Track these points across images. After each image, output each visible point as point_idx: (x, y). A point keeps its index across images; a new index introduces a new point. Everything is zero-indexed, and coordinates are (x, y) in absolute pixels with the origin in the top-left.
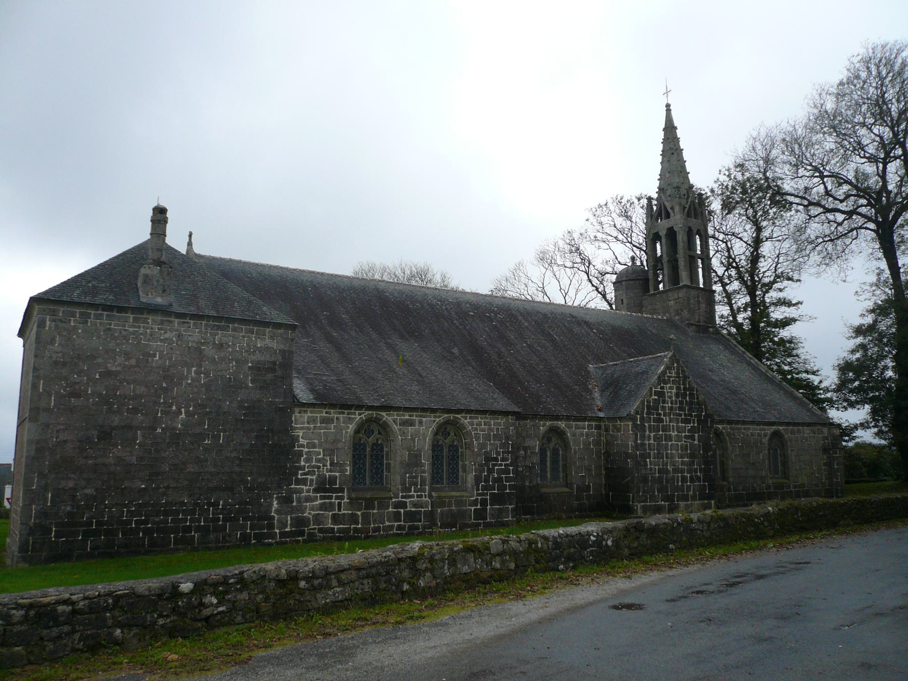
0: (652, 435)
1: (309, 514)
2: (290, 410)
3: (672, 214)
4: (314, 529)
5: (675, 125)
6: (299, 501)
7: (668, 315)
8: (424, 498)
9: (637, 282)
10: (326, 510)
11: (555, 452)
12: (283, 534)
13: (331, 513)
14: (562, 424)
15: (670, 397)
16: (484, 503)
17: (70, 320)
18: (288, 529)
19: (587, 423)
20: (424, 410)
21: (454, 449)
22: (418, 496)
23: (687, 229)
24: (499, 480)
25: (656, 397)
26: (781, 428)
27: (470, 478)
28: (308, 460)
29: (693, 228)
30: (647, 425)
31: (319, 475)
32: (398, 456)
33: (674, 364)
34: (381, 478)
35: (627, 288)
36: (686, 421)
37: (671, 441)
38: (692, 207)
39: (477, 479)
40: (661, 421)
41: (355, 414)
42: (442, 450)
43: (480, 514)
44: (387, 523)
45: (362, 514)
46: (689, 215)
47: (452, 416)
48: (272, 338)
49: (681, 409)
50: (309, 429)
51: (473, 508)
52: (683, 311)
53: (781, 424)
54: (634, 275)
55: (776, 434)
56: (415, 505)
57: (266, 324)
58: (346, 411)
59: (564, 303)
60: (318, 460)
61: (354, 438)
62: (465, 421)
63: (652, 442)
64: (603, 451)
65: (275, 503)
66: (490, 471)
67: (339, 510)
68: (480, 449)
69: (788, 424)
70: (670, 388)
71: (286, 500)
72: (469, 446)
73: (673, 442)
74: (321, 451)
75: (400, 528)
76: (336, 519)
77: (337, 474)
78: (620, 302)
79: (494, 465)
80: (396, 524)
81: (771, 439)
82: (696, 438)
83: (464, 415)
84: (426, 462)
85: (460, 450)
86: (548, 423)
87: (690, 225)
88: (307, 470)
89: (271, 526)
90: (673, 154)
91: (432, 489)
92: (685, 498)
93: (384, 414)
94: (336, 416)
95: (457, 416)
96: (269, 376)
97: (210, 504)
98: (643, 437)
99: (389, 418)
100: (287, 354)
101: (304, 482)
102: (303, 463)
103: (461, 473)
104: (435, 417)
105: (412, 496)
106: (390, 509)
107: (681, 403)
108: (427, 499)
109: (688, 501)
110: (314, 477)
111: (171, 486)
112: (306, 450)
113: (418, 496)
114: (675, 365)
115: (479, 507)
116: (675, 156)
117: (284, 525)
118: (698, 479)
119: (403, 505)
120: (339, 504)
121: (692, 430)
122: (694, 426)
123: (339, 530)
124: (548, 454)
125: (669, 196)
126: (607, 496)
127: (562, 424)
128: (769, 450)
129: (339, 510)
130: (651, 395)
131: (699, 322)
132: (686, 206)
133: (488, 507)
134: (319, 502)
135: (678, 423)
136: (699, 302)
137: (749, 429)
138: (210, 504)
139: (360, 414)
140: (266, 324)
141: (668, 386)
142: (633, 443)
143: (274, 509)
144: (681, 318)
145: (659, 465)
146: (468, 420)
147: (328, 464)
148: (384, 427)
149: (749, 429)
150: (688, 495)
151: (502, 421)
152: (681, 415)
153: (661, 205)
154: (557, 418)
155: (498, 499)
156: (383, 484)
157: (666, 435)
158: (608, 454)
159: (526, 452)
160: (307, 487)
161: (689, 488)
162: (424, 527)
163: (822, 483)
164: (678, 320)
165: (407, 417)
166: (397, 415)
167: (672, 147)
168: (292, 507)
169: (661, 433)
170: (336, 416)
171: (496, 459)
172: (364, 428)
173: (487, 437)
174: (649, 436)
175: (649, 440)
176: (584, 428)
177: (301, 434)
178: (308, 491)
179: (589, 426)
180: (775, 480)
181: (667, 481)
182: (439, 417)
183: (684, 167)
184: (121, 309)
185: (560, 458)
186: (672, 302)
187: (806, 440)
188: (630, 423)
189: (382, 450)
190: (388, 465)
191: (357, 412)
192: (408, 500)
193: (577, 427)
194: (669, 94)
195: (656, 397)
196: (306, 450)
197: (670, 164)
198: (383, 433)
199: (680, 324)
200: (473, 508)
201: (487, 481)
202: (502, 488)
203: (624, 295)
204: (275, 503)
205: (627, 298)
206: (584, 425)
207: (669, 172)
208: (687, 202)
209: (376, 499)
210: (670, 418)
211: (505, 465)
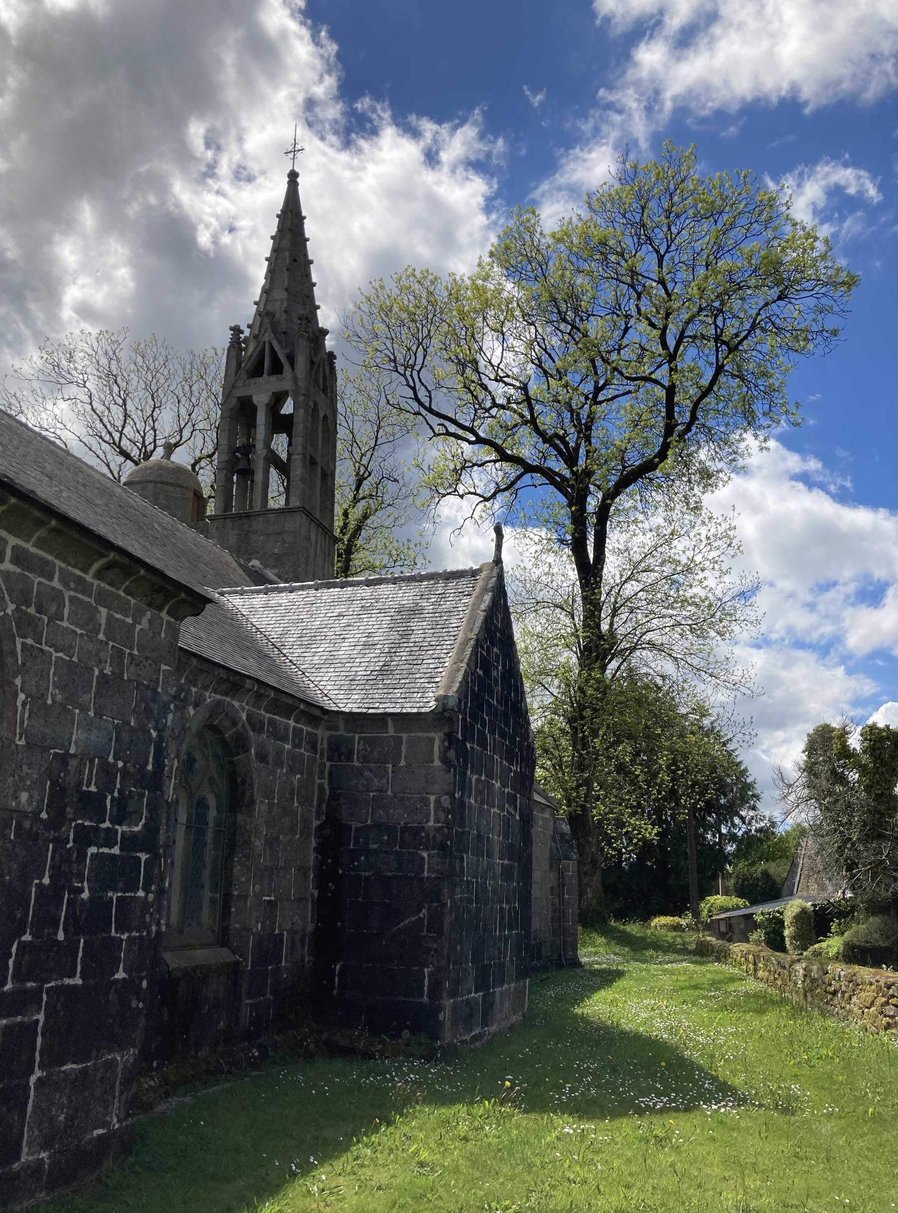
79: (85, 837)
127: (241, 708)
142: (446, 801)
153: (263, 350)
188: (437, 738)
211: (130, 842)
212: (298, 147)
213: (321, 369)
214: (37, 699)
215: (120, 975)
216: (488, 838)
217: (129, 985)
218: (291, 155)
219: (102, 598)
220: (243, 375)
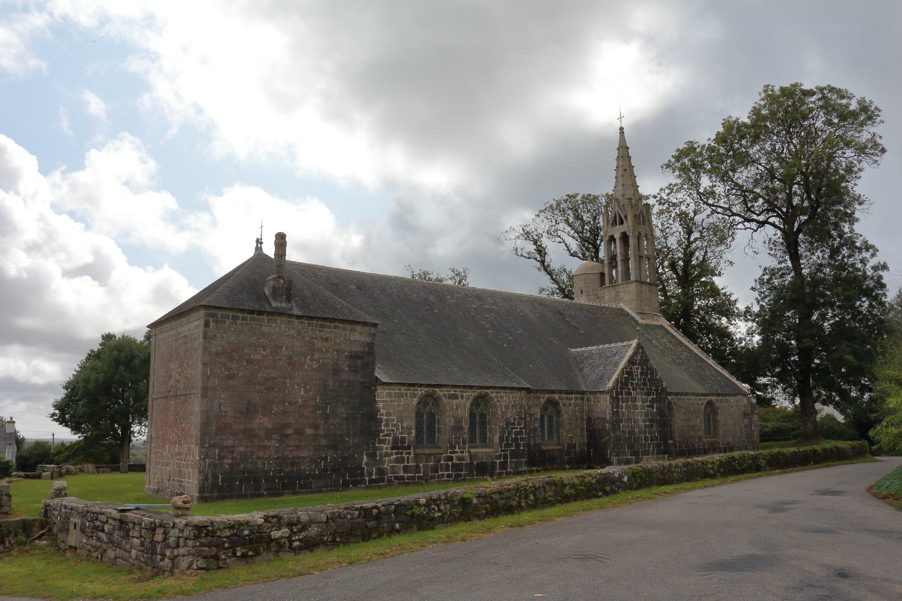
0: (624, 404)
1: (388, 465)
2: (375, 388)
3: (625, 221)
4: (392, 477)
6: (381, 456)
8: (464, 454)
10: (398, 463)
11: (550, 418)
12: (371, 481)
13: (402, 465)
14: (556, 396)
15: (637, 376)
16: (505, 457)
17: (226, 321)
18: (374, 477)
19: (574, 396)
20: (464, 387)
21: (483, 416)
22: (461, 452)
24: (516, 439)
25: (627, 376)
26: (713, 398)
27: (496, 439)
28: (387, 425)
30: (620, 397)
31: (394, 437)
32: (447, 422)
34: (434, 438)
36: (648, 394)
37: (637, 409)
38: (641, 216)
39: (501, 439)
40: (631, 394)
41: (418, 390)
42: (475, 417)
43: (503, 466)
44: (440, 473)
45: (423, 466)
47: (483, 391)
48: (361, 333)
49: (645, 384)
50: (386, 401)
51: (498, 461)
53: (713, 395)
55: (710, 403)
56: (459, 458)
57: (358, 323)
58: (412, 388)
60: (393, 426)
61: (417, 408)
62: (493, 394)
63: (624, 410)
64: (585, 418)
65: (365, 457)
66: (510, 433)
67: (408, 463)
68: (503, 417)
69: (718, 395)
70: (637, 369)
71: (372, 456)
72: (494, 414)
73: (639, 410)
74: (395, 418)
75: (448, 476)
76: (406, 469)
77: (406, 436)
78: (580, 292)
79: (512, 429)
80: (446, 473)
81: (706, 408)
82: (655, 407)
83: (491, 390)
84: (466, 426)
85: (488, 417)
86: (547, 396)
88: (386, 433)
89: (362, 474)
91: (470, 447)
92: (647, 453)
93: (437, 390)
94: (405, 392)
95: (487, 391)
96: (359, 362)
97: (322, 459)
98: (617, 407)
99: (441, 393)
100: (371, 345)
101: (383, 442)
102: (383, 428)
103: (488, 434)
104: (472, 392)
105: (457, 452)
106: (442, 462)
107: (645, 379)
108: (467, 454)
109: (649, 455)
110: (391, 438)
112: (385, 418)
113: (461, 452)
115: (502, 460)
117: (370, 474)
118: (656, 438)
119: (451, 459)
120: (408, 458)
121: (652, 401)
122: (653, 398)
123: (408, 478)
124: (546, 420)
126: (589, 451)
127: (556, 396)
128: (704, 416)
129: (408, 463)
130: (623, 374)
133: (509, 460)
134: (394, 456)
135: (642, 396)
137: (690, 399)
138: (322, 459)
139: (421, 390)
140: (358, 323)
141: (635, 367)
142: (610, 412)
143: (364, 462)
145: (628, 428)
146: (495, 394)
147: (400, 428)
148: (436, 400)
149: (690, 399)
150: (648, 451)
151: (518, 394)
152: (644, 389)
153: (616, 214)
154: (553, 392)
155: (514, 454)
156: (435, 443)
157: (633, 405)
158: (589, 419)
159: (531, 418)
160: (386, 446)
161: (649, 445)
162: (465, 475)
163: (742, 441)
165: (453, 392)
166: (447, 391)
168: (376, 460)
169: (630, 403)
170: (405, 392)
171: (513, 424)
172: (423, 402)
173: (507, 407)
174: (622, 405)
175: (622, 409)
176: (572, 399)
177: (381, 406)
178: (387, 449)
179: (576, 398)
180: (708, 440)
181: (635, 440)
182: (475, 392)
184: (260, 313)
185: (554, 423)
187: (732, 407)
188: (608, 396)
189: (434, 418)
190: (439, 429)
191: (419, 389)
192: (454, 455)
193: (567, 399)
194: (619, 117)
195: (627, 376)
196: (385, 418)
198: (435, 404)
200: (498, 461)
201: (507, 440)
202: (518, 446)
204: (365, 457)
206: (572, 397)
209: (432, 454)
210: (636, 392)
211: (520, 428)
212: (622, 116)
213: (641, 216)
214: (501, 411)
215: (522, 448)
216: (634, 419)
217: (523, 450)
218: (622, 116)
219: (510, 393)
220: (610, 225)
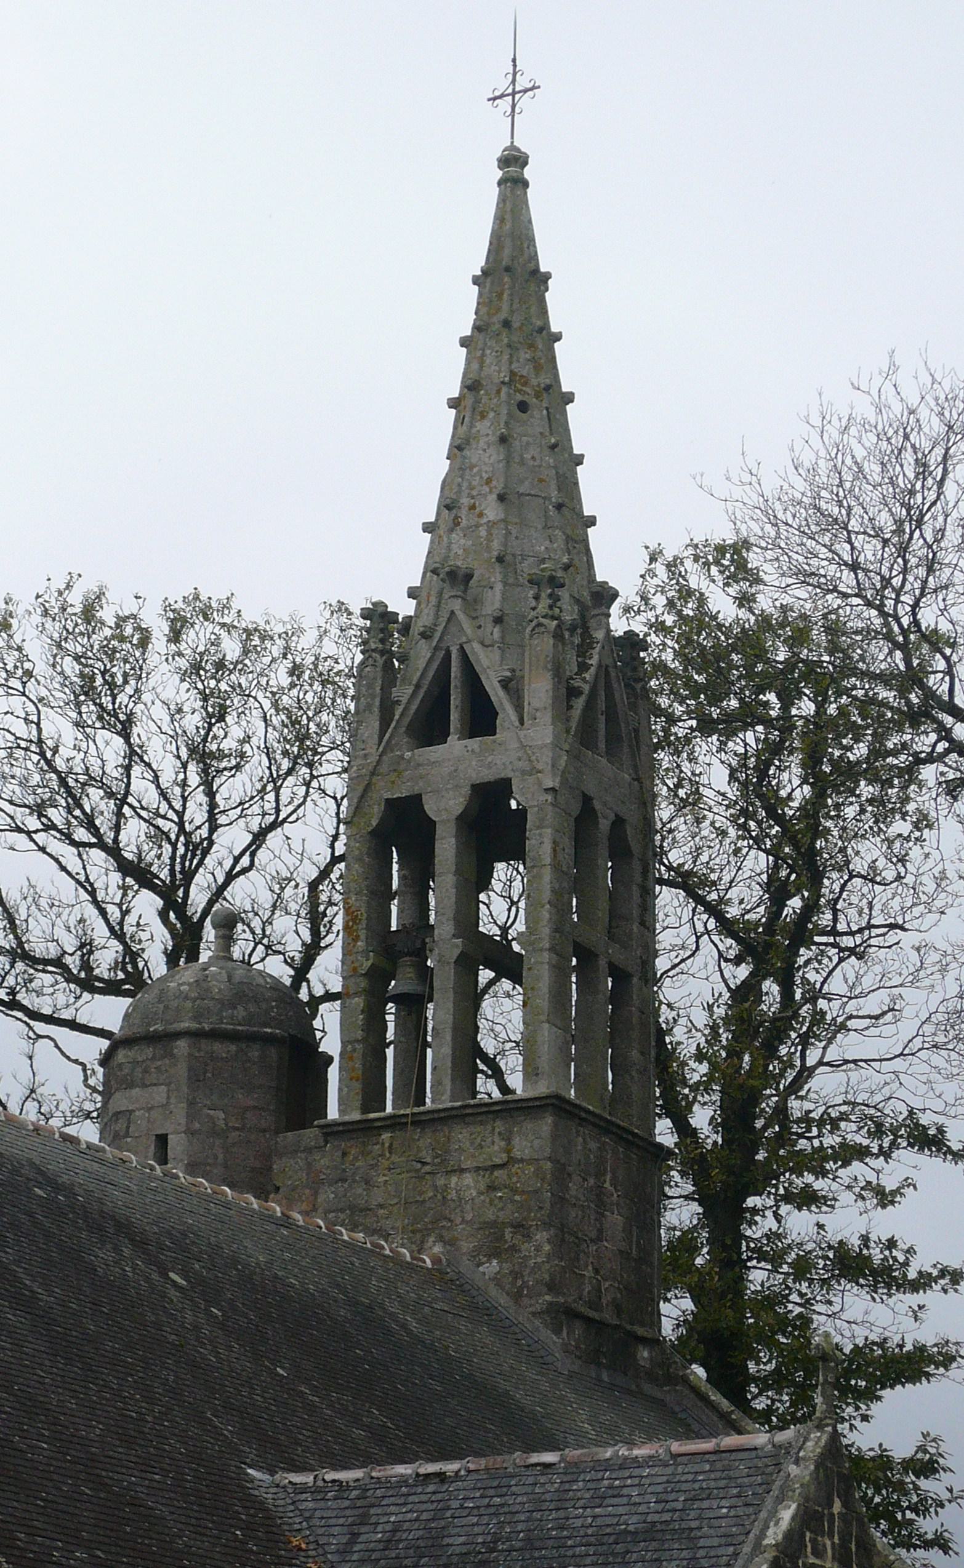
3: (506, 713)
5: (543, 269)
7: (437, 1249)
9: (255, 1053)
23: (576, 809)
29: (597, 805)
33: (830, 1505)
35: (196, 1078)
46: (585, 736)
52: (528, 1237)
54: (240, 1013)
59: (105, 1044)
87: (591, 789)
90: (523, 407)
111: (931, 579)
114: (837, 1507)
116: (537, 418)
125: (498, 620)
131: (595, 1305)
132: (577, 683)
136: (599, 1197)
144: (516, 1275)
153: (448, 654)
164: (497, 1280)
167: (526, 370)
183: (569, 488)
186: (468, 1179)
194: (524, 101)
197: (508, 460)
199: (503, 1300)
203: (180, 1111)
205: (190, 1132)
207: (501, 498)
208: (583, 667)
